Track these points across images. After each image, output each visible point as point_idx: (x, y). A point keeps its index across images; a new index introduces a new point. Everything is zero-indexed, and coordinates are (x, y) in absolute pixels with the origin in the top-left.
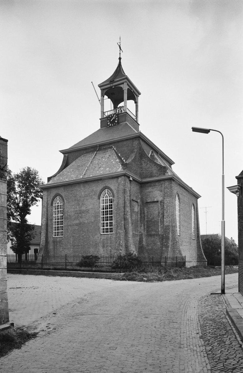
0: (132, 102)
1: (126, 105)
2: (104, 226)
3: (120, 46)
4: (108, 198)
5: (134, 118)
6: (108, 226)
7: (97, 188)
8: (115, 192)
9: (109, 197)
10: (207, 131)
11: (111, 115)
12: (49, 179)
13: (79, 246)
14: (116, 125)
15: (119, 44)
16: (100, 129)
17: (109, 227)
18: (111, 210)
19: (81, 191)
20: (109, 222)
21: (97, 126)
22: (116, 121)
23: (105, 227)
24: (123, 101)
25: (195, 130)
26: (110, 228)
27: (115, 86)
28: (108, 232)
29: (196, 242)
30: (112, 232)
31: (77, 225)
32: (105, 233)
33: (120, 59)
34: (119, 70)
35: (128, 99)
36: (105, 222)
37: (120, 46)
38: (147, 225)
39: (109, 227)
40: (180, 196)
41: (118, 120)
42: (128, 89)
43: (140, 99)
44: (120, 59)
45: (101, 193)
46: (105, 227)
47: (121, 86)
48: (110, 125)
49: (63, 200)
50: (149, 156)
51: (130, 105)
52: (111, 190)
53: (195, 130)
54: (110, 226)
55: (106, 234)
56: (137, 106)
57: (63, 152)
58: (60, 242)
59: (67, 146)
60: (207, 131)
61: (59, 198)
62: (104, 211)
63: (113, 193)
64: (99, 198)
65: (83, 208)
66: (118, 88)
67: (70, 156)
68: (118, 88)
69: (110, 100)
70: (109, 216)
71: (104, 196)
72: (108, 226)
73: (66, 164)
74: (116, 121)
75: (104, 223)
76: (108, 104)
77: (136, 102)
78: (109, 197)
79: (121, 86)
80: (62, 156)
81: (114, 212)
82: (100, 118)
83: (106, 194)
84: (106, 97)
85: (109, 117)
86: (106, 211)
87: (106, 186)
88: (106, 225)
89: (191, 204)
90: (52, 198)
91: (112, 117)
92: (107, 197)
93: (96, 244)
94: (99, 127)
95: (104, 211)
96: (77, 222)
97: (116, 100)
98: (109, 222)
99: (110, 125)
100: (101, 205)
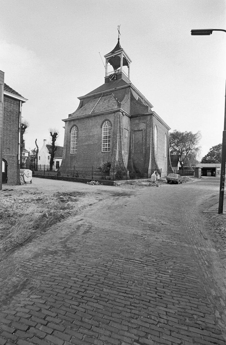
0: (126, 67)
1: (121, 68)
2: (104, 147)
3: (119, 31)
4: (108, 127)
5: (127, 77)
6: (107, 146)
7: (99, 120)
8: (112, 123)
9: (109, 126)
10: (208, 32)
11: (112, 74)
12: (70, 115)
13: (87, 160)
14: (115, 81)
15: (118, 29)
16: (104, 84)
17: (108, 147)
18: (109, 139)
19: (90, 122)
20: (108, 143)
21: (103, 82)
22: (115, 79)
23: (105, 147)
24: (120, 67)
25: (194, 32)
26: (108, 148)
27: (115, 56)
28: (107, 151)
29: (167, 159)
30: (110, 150)
31: (86, 145)
32: (105, 151)
33: (119, 39)
34: (118, 47)
35: (123, 65)
36: (105, 143)
37: (119, 31)
38: (134, 146)
39: (108, 147)
40: (158, 127)
41: (116, 78)
42: (124, 57)
43: (130, 65)
44: (119, 39)
45: (103, 124)
46: (105, 147)
47: (119, 56)
48: (111, 81)
49: (78, 129)
50: (137, 100)
51: (124, 69)
52: (110, 121)
53: (194, 32)
54: (108, 146)
55: (105, 152)
56: (129, 69)
57: (80, 98)
58: (75, 157)
59: (83, 94)
60: (208, 32)
61: (75, 128)
62: (104, 132)
63: (111, 123)
64: (101, 127)
65: (91, 134)
66: (116, 58)
67: (84, 101)
68: (116, 58)
69: (111, 66)
70: (108, 131)
71: (105, 126)
72: (107, 146)
73: (81, 105)
74: (115, 79)
75: (104, 144)
76: (111, 70)
77: (128, 67)
78: (109, 126)
79: (119, 56)
80: (79, 101)
81: (112, 136)
82: (105, 77)
83: (107, 124)
84: (109, 64)
85: (111, 76)
86: (107, 134)
87: (106, 119)
88: (106, 146)
89: (164, 133)
90: (70, 128)
91: (112, 76)
92: (107, 127)
93: (99, 159)
94: (104, 83)
95: (104, 148)
96: (87, 143)
97: (116, 66)
98: (108, 143)
99: (111, 81)
100: (103, 132)
